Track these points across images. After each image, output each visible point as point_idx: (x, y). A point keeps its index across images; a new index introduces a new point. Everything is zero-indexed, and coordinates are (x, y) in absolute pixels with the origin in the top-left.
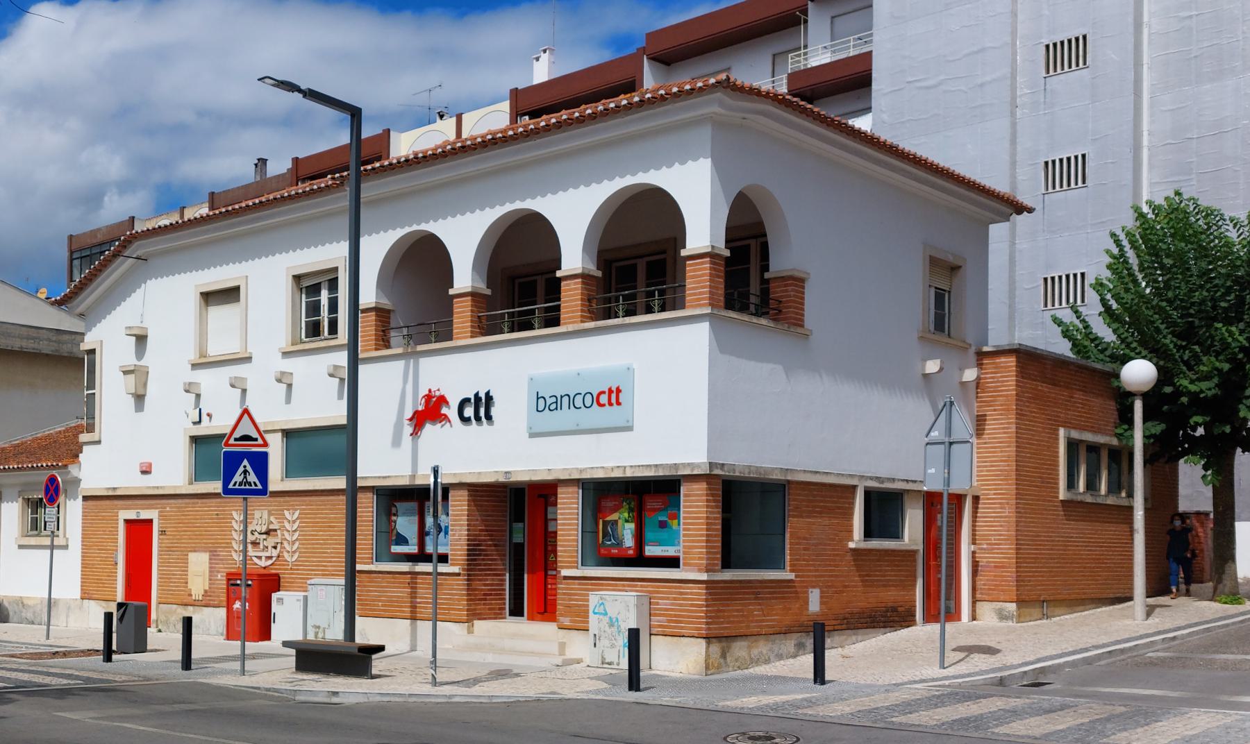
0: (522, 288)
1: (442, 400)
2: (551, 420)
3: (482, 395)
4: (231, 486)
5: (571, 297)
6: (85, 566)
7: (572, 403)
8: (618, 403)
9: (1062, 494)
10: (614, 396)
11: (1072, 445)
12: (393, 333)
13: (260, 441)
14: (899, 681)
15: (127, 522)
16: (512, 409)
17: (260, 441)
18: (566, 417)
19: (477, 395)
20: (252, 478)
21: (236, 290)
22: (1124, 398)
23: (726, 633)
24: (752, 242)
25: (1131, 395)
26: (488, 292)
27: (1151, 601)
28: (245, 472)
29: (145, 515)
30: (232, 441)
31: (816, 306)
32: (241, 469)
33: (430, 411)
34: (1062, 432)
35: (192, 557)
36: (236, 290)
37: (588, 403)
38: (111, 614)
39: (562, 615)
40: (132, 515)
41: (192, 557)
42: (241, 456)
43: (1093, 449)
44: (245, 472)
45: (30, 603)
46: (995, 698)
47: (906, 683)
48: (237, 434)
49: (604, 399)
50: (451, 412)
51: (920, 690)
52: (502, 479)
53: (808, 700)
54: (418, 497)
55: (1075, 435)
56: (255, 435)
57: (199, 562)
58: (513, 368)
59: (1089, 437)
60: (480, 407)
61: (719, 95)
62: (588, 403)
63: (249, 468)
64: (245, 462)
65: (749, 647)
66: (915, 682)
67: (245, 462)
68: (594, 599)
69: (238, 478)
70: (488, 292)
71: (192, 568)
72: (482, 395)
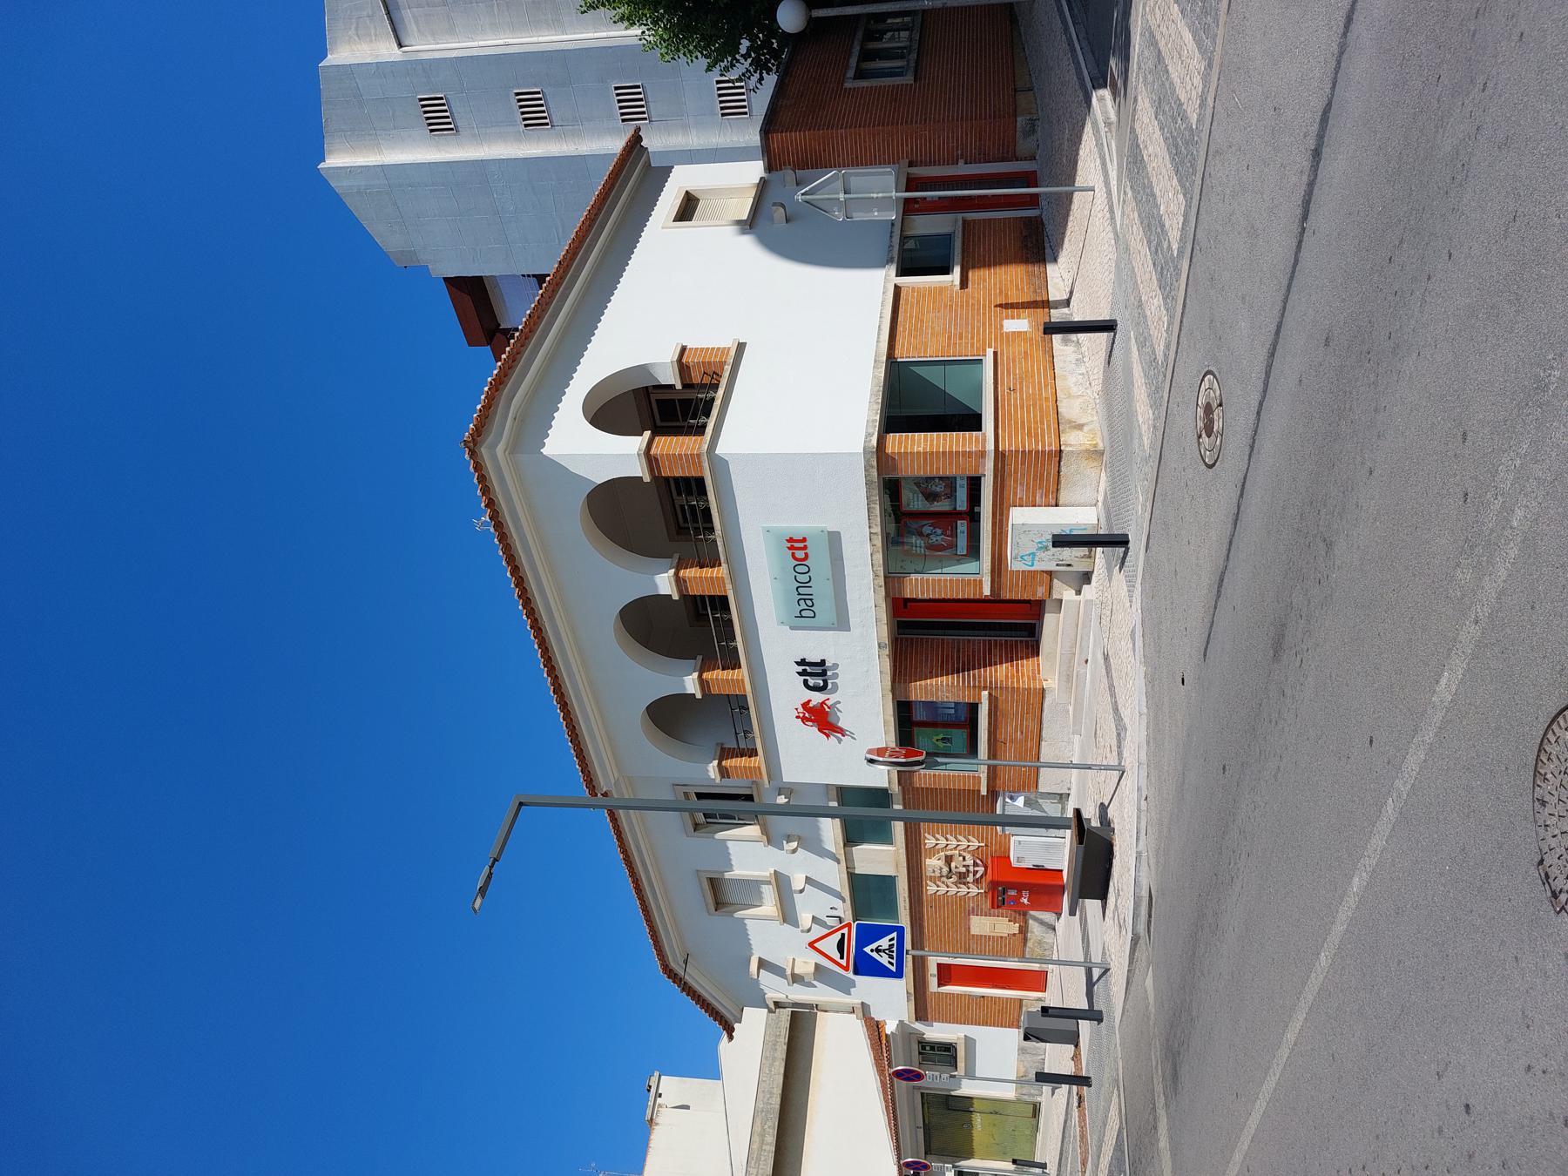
0: (699, 627)
1: (805, 705)
2: (824, 606)
3: (800, 669)
4: (893, 969)
5: (700, 579)
6: (985, 1024)
7: (806, 585)
8: (804, 540)
9: (908, 79)
10: (797, 545)
11: (860, 75)
12: (742, 746)
13: (845, 931)
14: (1111, 235)
15: (940, 985)
16: (816, 645)
17: (845, 931)
18: (821, 588)
19: (800, 674)
20: (884, 943)
21: (711, 881)
22: (814, 29)
23: (1053, 426)
24: (653, 398)
25: (811, 22)
26: (700, 658)
27: (978, 577)
28: (878, 950)
29: (933, 970)
30: (843, 962)
31: (708, 337)
32: (874, 955)
33: (821, 719)
34: (848, 85)
35: (975, 931)
36: (711, 881)
37: (805, 569)
38: (1037, 981)
39: (1035, 594)
40: (933, 982)
41: (975, 931)
42: (860, 953)
43: (867, 56)
44: (878, 950)
45: (1022, 1070)
46: (1137, 126)
47: (1115, 228)
48: (836, 956)
49: (800, 554)
50: (817, 698)
51: (1129, 217)
52: (887, 651)
53: (1141, 345)
54: (907, 719)
55: (851, 73)
56: (837, 936)
57: (981, 925)
58: (776, 644)
59: (853, 61)
60: (815, 673)
61: (484, 451)
62: (805, 569)
63: (873, 946)
64: (867, 950)
65: (1070, 396)
66: (1112, 218)
67: (867, 950)
68: (1014, 565)
69: (884, 959)
70: (700, 658)
71: (987, 931)
72: (800, 669)
